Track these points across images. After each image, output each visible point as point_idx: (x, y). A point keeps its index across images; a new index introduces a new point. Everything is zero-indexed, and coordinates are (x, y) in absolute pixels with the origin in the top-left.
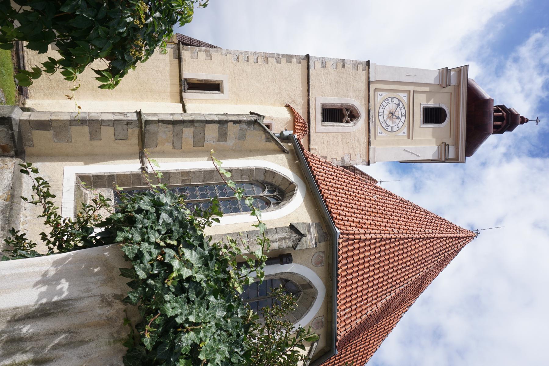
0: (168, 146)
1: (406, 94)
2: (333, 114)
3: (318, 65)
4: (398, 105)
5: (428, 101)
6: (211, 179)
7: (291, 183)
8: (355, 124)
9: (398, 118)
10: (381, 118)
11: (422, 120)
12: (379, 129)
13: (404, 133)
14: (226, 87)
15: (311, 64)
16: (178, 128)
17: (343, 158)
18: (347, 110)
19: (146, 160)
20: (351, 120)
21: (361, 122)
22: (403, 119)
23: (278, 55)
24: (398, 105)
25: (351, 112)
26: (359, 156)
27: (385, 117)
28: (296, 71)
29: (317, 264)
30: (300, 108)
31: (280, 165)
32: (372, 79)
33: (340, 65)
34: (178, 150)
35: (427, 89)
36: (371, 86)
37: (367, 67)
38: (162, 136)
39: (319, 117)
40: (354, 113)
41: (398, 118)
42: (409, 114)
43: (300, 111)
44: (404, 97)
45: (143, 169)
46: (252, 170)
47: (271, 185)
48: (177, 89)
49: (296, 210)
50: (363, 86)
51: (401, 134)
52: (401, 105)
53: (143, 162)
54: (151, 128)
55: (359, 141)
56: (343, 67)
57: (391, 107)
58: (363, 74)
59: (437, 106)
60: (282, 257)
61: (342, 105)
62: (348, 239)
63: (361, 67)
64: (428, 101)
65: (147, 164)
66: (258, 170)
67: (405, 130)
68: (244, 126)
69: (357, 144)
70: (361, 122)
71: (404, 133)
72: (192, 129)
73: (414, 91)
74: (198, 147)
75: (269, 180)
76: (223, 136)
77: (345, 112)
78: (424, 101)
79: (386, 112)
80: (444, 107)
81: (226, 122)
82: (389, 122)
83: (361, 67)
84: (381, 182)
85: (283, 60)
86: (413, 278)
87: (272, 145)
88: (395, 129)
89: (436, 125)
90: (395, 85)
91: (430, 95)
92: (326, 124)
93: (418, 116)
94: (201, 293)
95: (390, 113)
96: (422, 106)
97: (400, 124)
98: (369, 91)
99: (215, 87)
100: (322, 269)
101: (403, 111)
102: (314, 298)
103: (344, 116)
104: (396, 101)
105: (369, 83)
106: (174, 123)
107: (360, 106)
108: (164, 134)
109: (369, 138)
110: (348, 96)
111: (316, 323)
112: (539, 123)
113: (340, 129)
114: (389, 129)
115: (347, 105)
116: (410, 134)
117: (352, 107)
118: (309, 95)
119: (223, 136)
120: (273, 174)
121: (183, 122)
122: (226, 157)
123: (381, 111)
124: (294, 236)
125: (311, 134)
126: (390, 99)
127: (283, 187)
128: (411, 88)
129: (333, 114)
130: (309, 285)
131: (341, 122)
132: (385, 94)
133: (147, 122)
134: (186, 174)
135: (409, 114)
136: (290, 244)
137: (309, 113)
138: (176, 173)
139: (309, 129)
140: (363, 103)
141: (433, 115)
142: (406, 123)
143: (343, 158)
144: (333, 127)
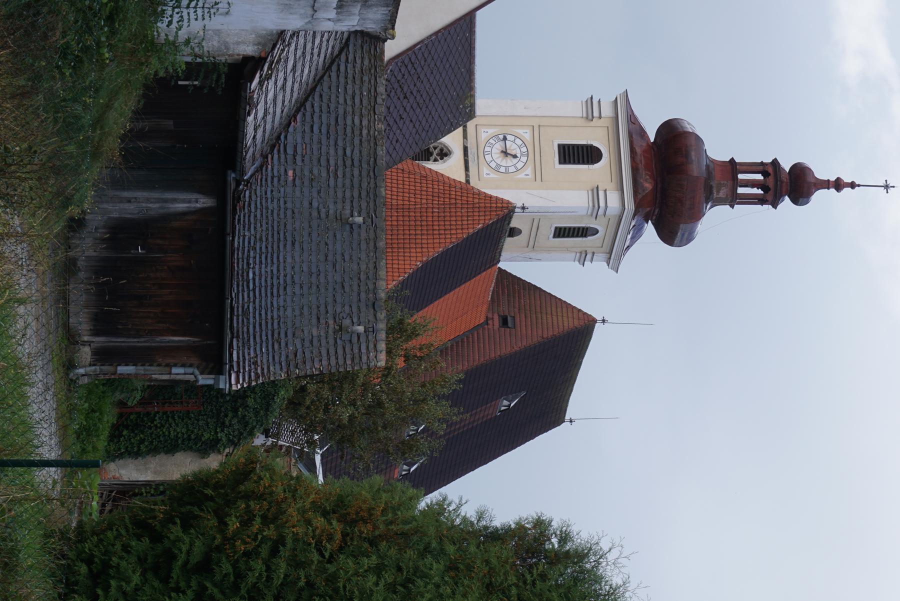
10: (488, 158)
12: (485, 170)
20: (442, 159)
25: (442, 150)
40: (445, 151)
51: (521, 176)
77: (438, 158)
80: (595, 144)
103: (432, 154)
112: (606, 318)
142: (531, 162)
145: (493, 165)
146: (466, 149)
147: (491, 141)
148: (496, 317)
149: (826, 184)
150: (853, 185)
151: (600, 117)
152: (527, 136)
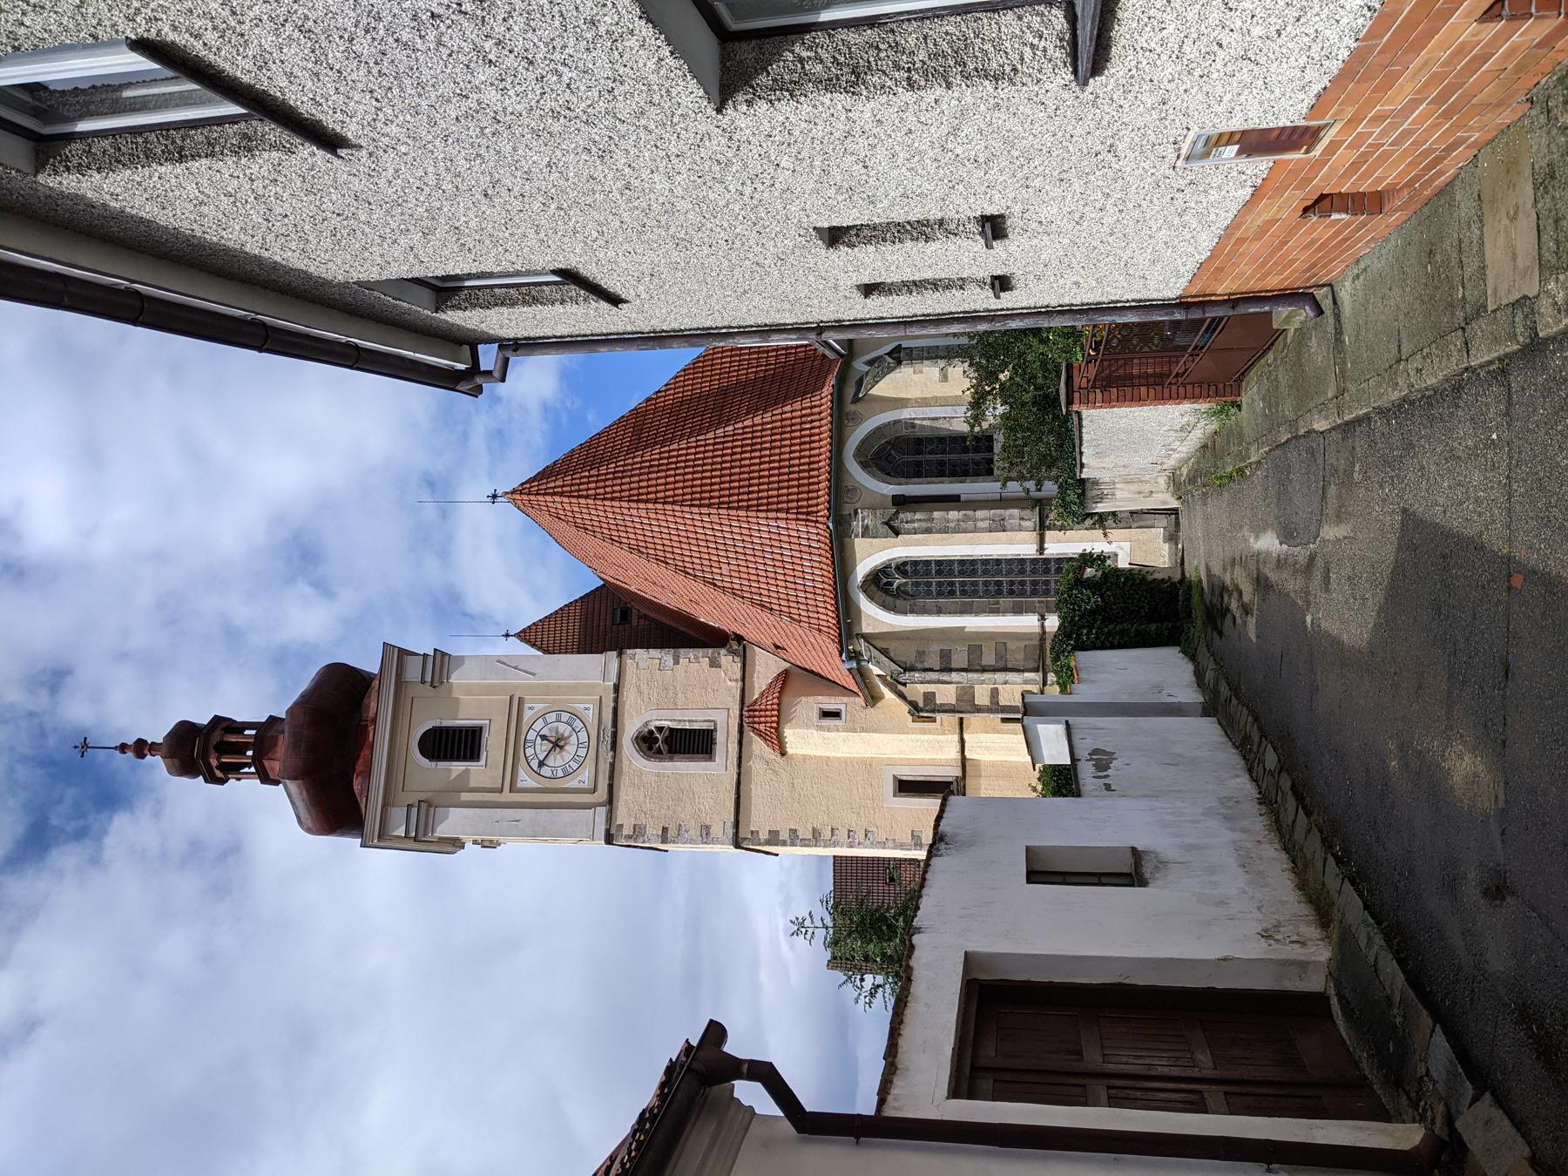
0: (1011, 645)
1: (520, 785)
2: (691, 743)
3: (716, 830)
4: (541, 764)
5: (467, 771)
6: (964, 604)
7: (865, 592)
8: (646, 724)
9: (544, 738)
10: (583, 737)
11: (485, 735)
12: (591, 716)
14: (889, 787)
15: (730, 832)
16: (1001, 664)
17: (677, 662)
18: (659, 751)
19: (1038, 630)
20: (651, 732)
21: (632, 727)
22: (532, 736)
23: (793, 844)
24: (541, 764)
25: (650, 749)
26: (642, 665)
27: (573, 739)
28: (760, 819)
29: (855, 489)
30: (757, 752)
31: (875, 617)
32: (602, 811)
33: (671, 833)
34: (1001, 641)
35: (465, 797)
36: (605, 797)
37: (613, 831)
38: (1020, 656)
39: (720, 737)
41: (544, 738)
42: (516, 745)
43: (758, 746)
44: (525, 779)
45: (1043, 618)
46: (912, 612)
47: (887, 592)
48: (968, 782)
49: (870, 555)
50: (624, 795)
51: (538, 706)
52: (535, 764)
53: (1043, 627)
54: (1031, 665)
55: (640, 692)
56: (665, 830)
57: (557, 760)
58: (623, 817)
59: (442, 765)
60: (901, 502)
61: (671, 760)
62: (808, 514)
63: (627, 831)
64: (467, 771)
65: (1037, 623)
66: (904, 613)
67: (528, 715)
68: (919, 666)
69: (644, 687)
70: (632, 727)
72: (984, 663)
73: (501, 791)
74: (975, 644)
75: (889, 599)
76: (945, 656)
77: (664, 748)
78: (478, 772)
79: (571, 749)
80: (425, 762)
81: (941, 670)
82: (564, 729)
83: (627, 831)
84: (507, 635)
85: (784, 835)
86: (675, 446)
87: (879, 644)
88: (551, 717)
89: (446, 723)
90: (552, 799)
91: (461, 785)
92: (704, 726)
93: (493, 744)
94: (47, 122)
95: (561, 747)
96: (482, 762)
97: (539, 725)
98: (611, 787)
99: (906, 787)
100: (848, 483)
101: (530, 752)
102: (859, 449)
103: (666, 741)
104: (546, 771)
105: (610, 801)
106: (1006, 669)
107: (633, 760)
108: (1017, 658)
109: (616, 700)
110: (658, 775)
111: (858, 419)
113: (678, 715)
114: (565, 717)
115: (661, 760)
116: (516, 706)
117: (648, 757)
118: (739, 775)
119: (945, 656)
120: (886, 607)
121: (995, 670)
122: (1020, 563)
123: (582, 752)
124: (895, 524)
125: (737, 707)
126: (560, 774)
127: (873, 588)
128: (507, 796)
129: (691, 743)
130: (864, 465)
131: (672, 730)
132: (573, 783)
133: (1037, 670)
134: (995, 611)
135: (516, 745)
136: (901, 516)
137: (740, 743)
138: (1005, 612)
139: (741, 715)
140: (625, 762)
141: (456, 744)
142: (525, 729)
143: (677, 662)
144: (691, 718)
146: (614, 746)
147: (575, 766)
148: (634, 623)
149: (153, 748)
150: (123, 748)
151: (410, 806)
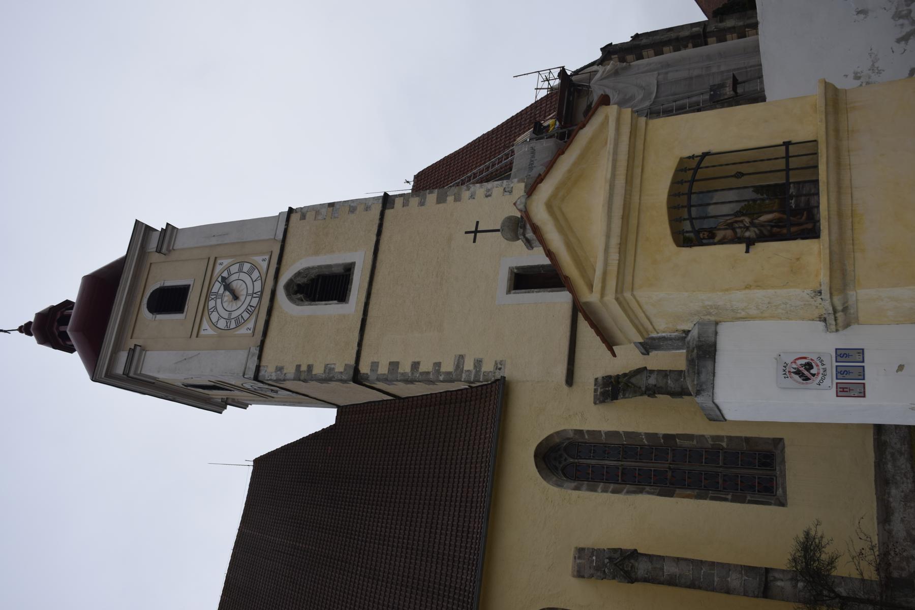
13: (221, 264)
71: (221, 264)
85: (318, 370)
123: (255, 302)
145: (256, 274)
152: (205, 325)
